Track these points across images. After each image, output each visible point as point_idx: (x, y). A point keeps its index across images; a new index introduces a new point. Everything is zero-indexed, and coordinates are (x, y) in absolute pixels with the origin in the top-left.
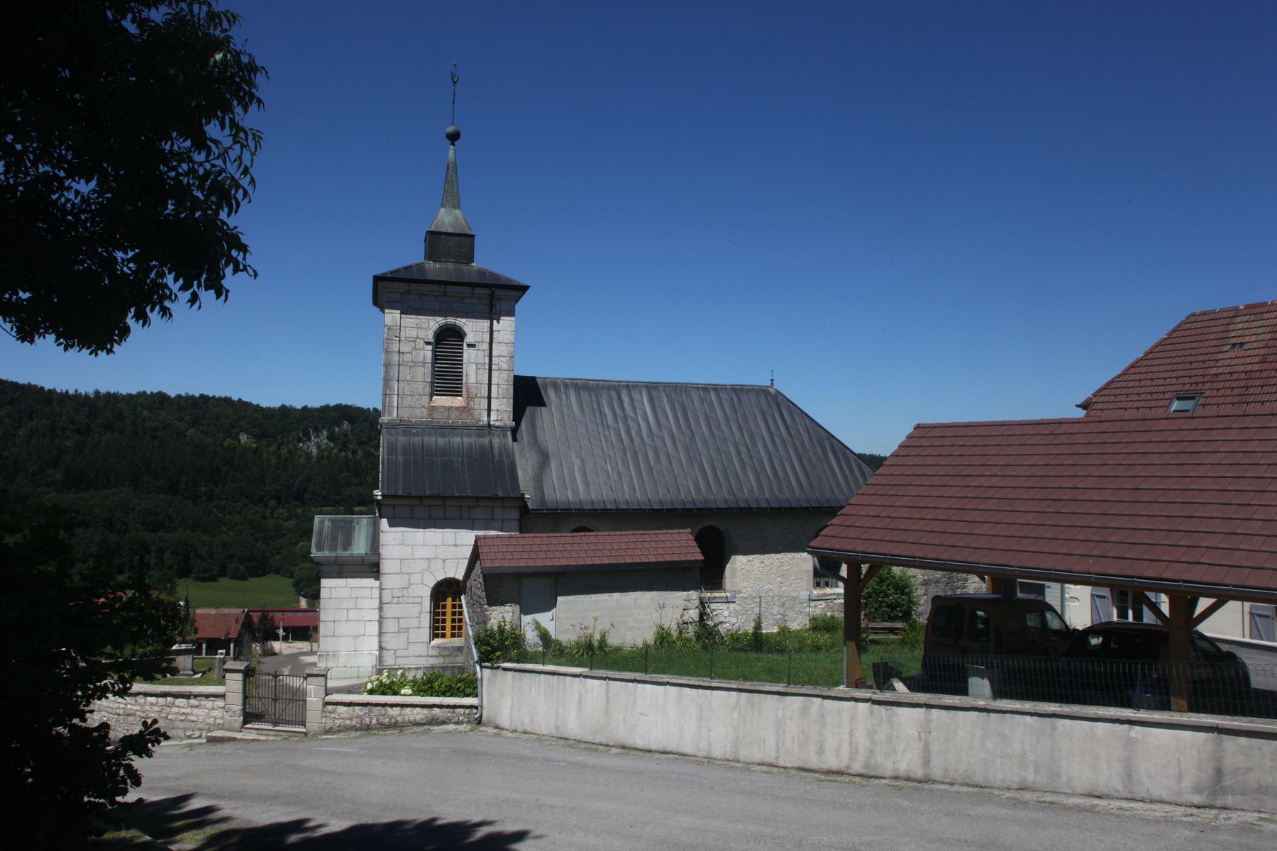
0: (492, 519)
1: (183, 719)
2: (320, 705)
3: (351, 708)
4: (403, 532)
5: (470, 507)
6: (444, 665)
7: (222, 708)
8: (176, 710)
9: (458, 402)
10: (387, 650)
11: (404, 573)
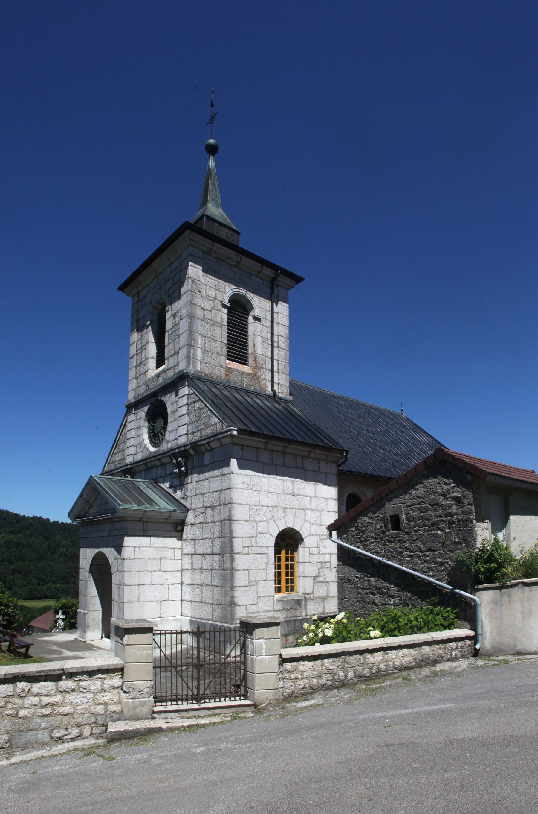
0: (319, 471)
1: (47, 712)
2: (276, 664)
3: (318, 662)
4: (250, 475)
5: (303, 457)
6: (288, 619)
7: (118, 688)
8: (35, 700)
9: (246, 369)
10: (239, 605)
11: (252, 521)
